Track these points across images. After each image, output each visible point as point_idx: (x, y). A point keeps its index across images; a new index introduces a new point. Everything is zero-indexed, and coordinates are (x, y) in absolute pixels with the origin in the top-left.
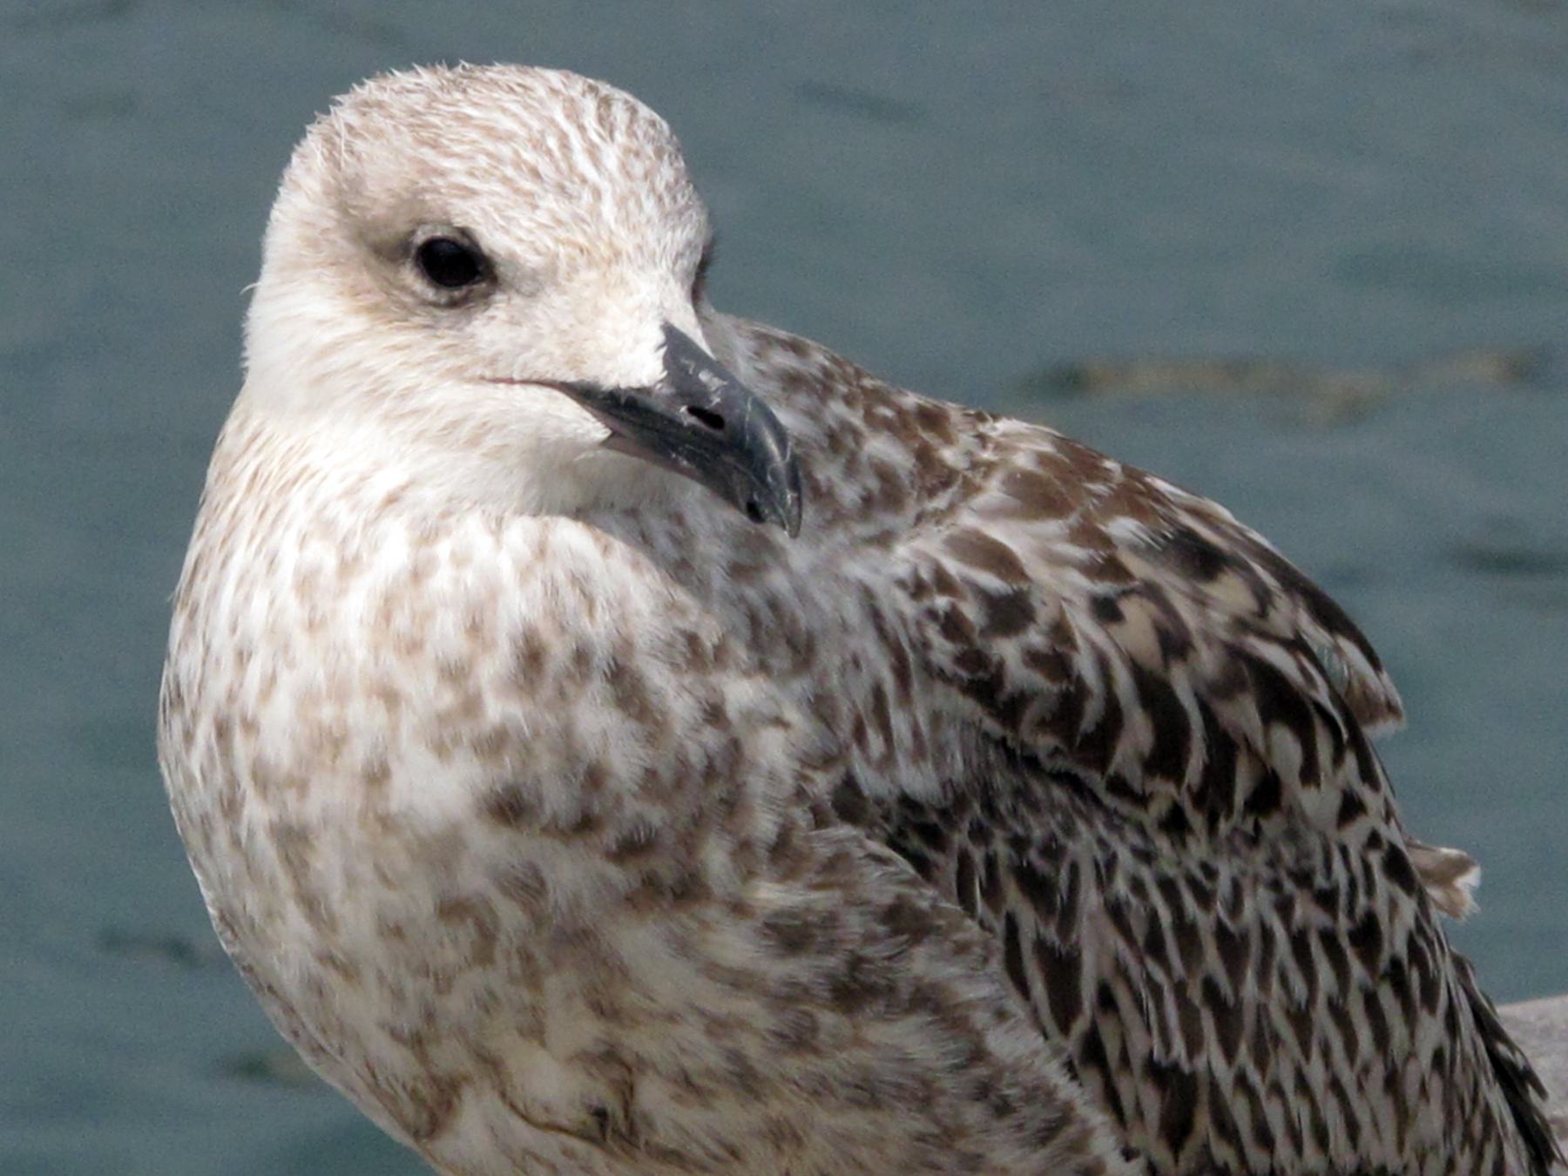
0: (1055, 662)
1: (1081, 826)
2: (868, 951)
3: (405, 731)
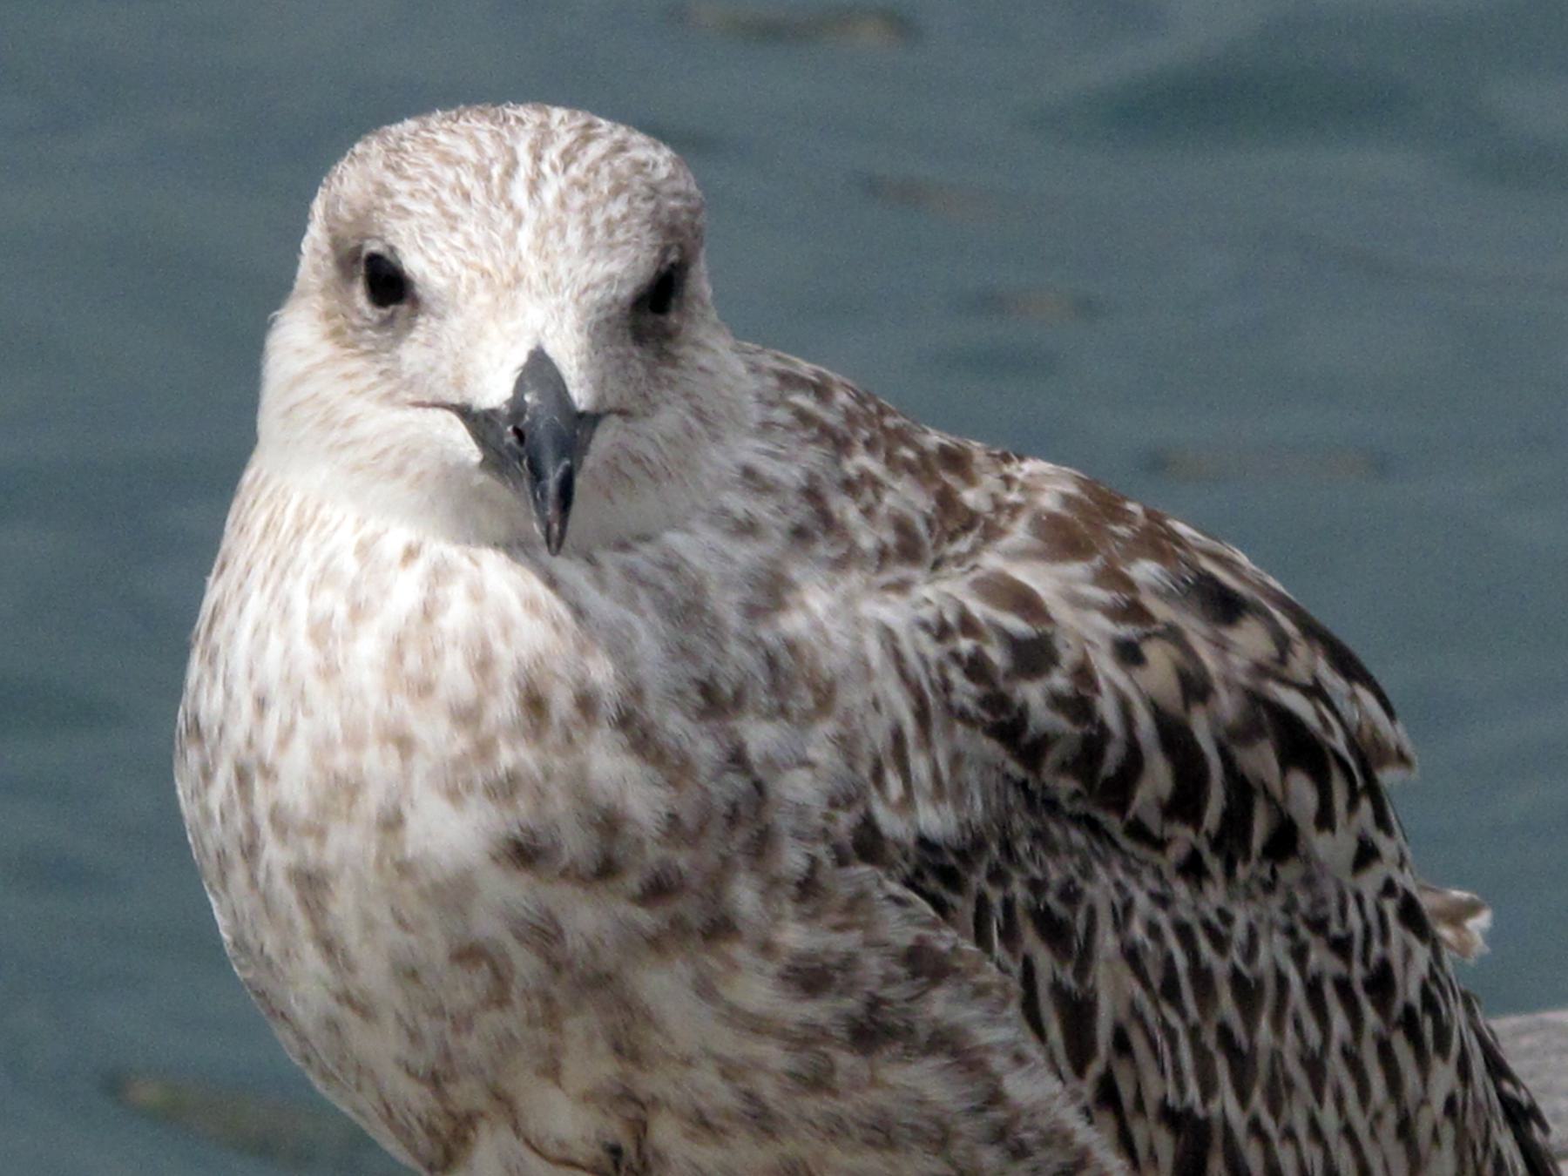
0: (1078, 705)
1: (1099, 870)
2: (890, 992)
3: (418, 779)
